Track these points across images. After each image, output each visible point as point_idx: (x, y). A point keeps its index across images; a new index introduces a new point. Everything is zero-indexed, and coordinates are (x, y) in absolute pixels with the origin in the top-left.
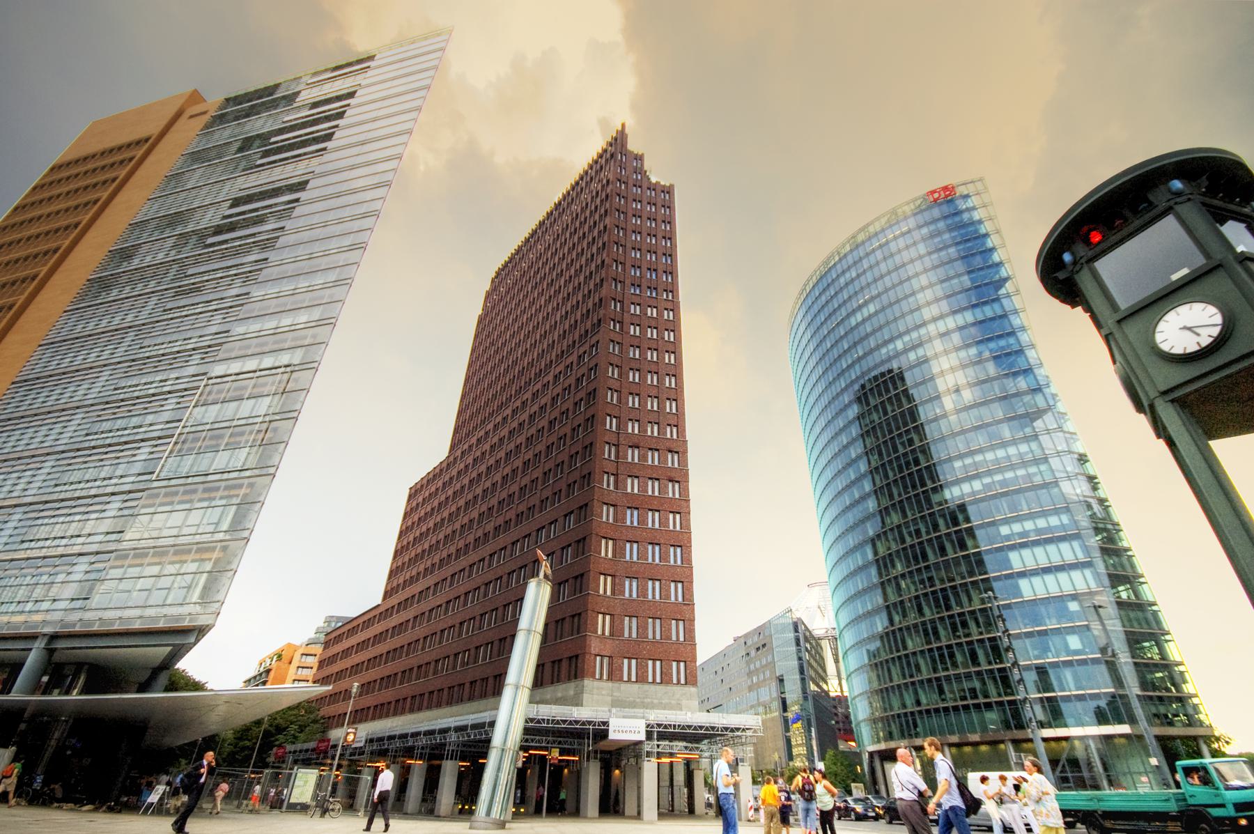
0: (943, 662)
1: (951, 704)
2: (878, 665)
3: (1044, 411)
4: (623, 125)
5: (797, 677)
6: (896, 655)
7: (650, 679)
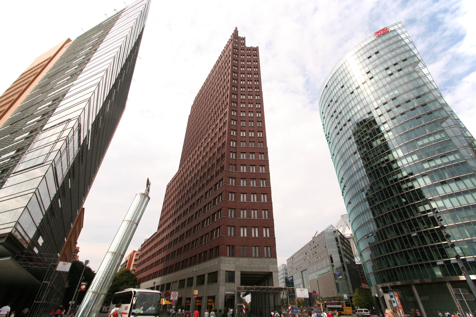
0: (407, 243)
1: (413, 264)
2: (372, 247)
3: (446, 118)
4: (236, 28)
5: (338, 255)
6: (382, 241)
7: (254, 256)
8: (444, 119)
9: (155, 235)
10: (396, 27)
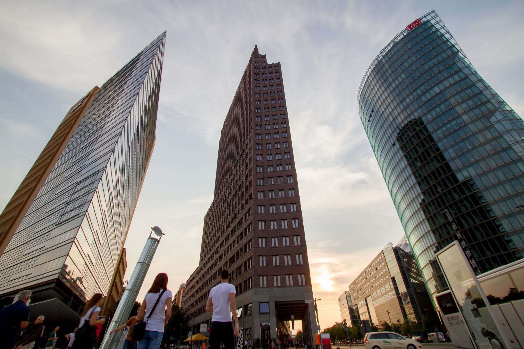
4: (256, 46)
8: (492, 113)
9: (198, 270)
10: (429, 17)
